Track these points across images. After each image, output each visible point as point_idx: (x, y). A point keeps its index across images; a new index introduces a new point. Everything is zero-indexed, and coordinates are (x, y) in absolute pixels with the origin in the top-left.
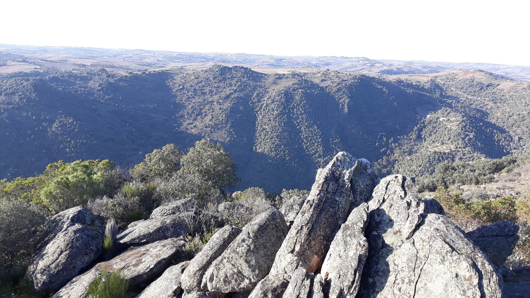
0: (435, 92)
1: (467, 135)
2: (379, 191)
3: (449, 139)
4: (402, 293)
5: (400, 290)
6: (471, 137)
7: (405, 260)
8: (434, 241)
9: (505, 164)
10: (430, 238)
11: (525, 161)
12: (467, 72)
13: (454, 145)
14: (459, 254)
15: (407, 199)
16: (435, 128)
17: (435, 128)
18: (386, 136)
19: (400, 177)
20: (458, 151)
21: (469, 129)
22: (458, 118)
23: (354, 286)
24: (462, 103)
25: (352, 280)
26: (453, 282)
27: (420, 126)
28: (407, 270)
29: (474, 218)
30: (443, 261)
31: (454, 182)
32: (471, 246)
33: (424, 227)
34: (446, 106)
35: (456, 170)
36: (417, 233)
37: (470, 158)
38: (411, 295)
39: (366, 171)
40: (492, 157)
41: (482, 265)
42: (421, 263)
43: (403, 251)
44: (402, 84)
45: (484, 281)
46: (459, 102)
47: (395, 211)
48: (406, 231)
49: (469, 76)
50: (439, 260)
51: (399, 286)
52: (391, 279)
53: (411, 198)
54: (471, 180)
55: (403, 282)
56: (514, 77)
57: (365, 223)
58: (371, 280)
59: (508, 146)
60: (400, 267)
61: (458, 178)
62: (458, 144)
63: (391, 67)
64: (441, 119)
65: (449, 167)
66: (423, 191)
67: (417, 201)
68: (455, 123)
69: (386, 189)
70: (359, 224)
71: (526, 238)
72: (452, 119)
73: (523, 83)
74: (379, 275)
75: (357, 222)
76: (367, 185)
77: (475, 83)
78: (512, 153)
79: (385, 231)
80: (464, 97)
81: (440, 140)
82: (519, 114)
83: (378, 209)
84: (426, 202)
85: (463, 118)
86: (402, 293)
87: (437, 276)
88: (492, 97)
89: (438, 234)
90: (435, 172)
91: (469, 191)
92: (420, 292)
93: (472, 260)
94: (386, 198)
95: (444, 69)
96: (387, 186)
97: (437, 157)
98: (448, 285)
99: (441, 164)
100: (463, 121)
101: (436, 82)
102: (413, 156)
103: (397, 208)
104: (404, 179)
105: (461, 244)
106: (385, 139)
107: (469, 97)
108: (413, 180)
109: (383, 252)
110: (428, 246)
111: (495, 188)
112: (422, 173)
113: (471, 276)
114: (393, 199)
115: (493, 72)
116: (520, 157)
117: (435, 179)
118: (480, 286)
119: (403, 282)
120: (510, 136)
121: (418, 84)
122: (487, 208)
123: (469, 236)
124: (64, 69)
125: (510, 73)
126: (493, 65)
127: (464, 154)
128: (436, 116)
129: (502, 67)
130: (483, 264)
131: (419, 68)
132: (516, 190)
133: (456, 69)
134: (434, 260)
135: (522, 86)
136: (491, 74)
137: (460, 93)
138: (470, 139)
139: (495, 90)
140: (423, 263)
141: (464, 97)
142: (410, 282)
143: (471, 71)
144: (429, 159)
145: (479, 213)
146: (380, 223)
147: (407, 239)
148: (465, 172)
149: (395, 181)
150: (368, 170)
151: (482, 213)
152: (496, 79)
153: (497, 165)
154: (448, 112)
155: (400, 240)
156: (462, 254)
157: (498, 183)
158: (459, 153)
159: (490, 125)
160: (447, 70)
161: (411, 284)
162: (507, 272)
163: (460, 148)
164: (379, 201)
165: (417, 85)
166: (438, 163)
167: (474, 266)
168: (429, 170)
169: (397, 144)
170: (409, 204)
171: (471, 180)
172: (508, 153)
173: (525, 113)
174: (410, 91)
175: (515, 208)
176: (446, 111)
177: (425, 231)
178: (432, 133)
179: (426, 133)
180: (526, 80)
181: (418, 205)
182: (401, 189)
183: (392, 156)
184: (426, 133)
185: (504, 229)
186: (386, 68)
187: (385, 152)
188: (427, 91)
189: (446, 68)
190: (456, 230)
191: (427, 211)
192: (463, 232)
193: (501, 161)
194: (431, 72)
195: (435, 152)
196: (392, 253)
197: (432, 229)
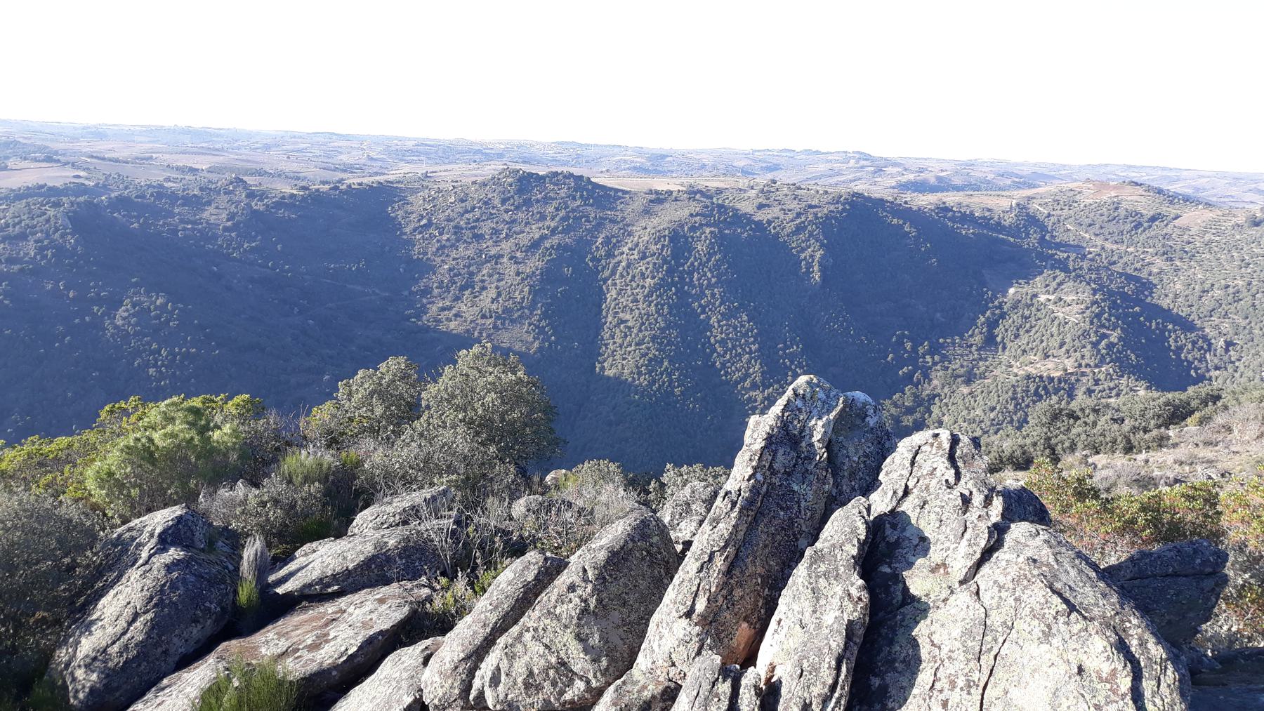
0: (1028, 235)
2: (894, 470)
3: (1062, 345)
6: (1114, 339)
7: (956, 632)
8: (1026, 588)
9: (1194, 404)
11: (1242, 399)
12: (1102, 185)
13: (1072, 360)
14: (1085, 618)
15: (963, 487)
16: (1027, 318)
17: (1027, 318)
18: (910, 339)
19: (945, 435)
20: (1083, 374)
21: (1109, 320)
23: (836, 695)
24: (1092, 260)
25: (830, 681)
26: (1072, 686)
27: (993, 314)
28: (961, 658)
29: (1121, 532)
30: (1047, 635)
31: (1073, 448)
32: (1115, 599)
33: (1001, 556)
34: (1053, 268)
35: (1077, 418)
36: (985, 569)
37: (1111, 389)
39: (863, 420)
41: (1141, 645)
42: (995, 640)
43: (953, 611)
44: (950, 214)
47: (933, 516)
49: (1106, 197)
50: (1037, 633)
51: (942, 697)
52: (924, 678)
54: (1114, 442)
55: (953, 685)
56: (1214, 199)
57: (862, 545)
58: (876, 682)
59: (1200, 361)
60: (945, 650)
61: (1083, 437)
62: (1083, 357)
64: (1042, 298)
66: (1000, 469)
67: (986, 492)
68: (1076, 308)
69: (913, 463)
70: (847, 547)
71: (1245, 581)
72: (1069, 298)
73: (1234, 211)
74: (895, 670)
76: (866, 456)
77: (1122, 212)
78: (1210, 379)
79: (910, 565)
81: (1041, 348)
82: (1227, 287)
83: (893, 511)
84: (1007, 495)
85: (1094, 295)
87: (1035, 671)
88: (1163, 246)
89: (1036, 572)
91: (1109, 468)
93: (1117, 634)
94: (911, 485)
95: (1047, 178)
96: (914, 458)
97: (1032, 388)
99: (1042, 406)
100: (1094, 303)
102: (977, 386)
103: (937, 510)
104: (955, 441)
105: (1090, 594)
106: (908, 346)
107: (1108, 246)
108: (976, 442)
109: (904, 615)
110: (1011, 601)
112: (997, 426)
114: (927, 488)
116: (1230, 387)
117: (1028, 441)
119: (953, 685)
120: (1205, 338)
121: (987, 214)
122: (1152, 509)
123: (1108, 575)
126: (1164, 169)
127: (1097, 382)
128: (1030, 290)
129: (1186, 173)
130: (1143, 644)
131: (990, 177)
132: (1220, 466)
133: (1076, 181)
134: (1026, 635)
136: (1160, 191)
137: (1087, 236)
138: (1110, 346)
139: (1168, 230)
140: (1001, 640)
141: (1096, 246)
142: (969, 685)
144: (1015, 393)
145: (1133, 521)
146: (897, 544)
147: (962, 583)
149: (932, 445)
150: (868, 419)
151: (1141, 521)
152: (1171, 202)
153: (1176, 408)
154: (1058, 280)
155: (944, 585)
156: (1092, 619)
157: (1177, 450)
158: (1084, 379)
161: (972, 691)
162: (1200, 662)
163: (1087, 365)
164: (895, 493)
165: (984, 218)
166: (1034, 402)
167: (1122, 646)
168: (1015, 418)
169: (937, 358)
170: (966, 501)
171: (1114, 442)
172: (1201, 379)
173: (1240, 282)
174: (967, 231)
175: (1219, 508)
176: (1054, 278)
177: (1004, 563)
178: (1022, 332)
180: (1241, 205)
181: (988, 501)
182: (947, 464)
185: (1193, 559)
186: (911, 177)
187: (910, 376)
188: (1008, 230)
189: (1053, 177)
190: (1077, 562)
191: (1010, 515)
192: (1094, 567)
193: (1184, 396)
194: (1019, 186)
195: (1028, 377)
197: (1021, 559)
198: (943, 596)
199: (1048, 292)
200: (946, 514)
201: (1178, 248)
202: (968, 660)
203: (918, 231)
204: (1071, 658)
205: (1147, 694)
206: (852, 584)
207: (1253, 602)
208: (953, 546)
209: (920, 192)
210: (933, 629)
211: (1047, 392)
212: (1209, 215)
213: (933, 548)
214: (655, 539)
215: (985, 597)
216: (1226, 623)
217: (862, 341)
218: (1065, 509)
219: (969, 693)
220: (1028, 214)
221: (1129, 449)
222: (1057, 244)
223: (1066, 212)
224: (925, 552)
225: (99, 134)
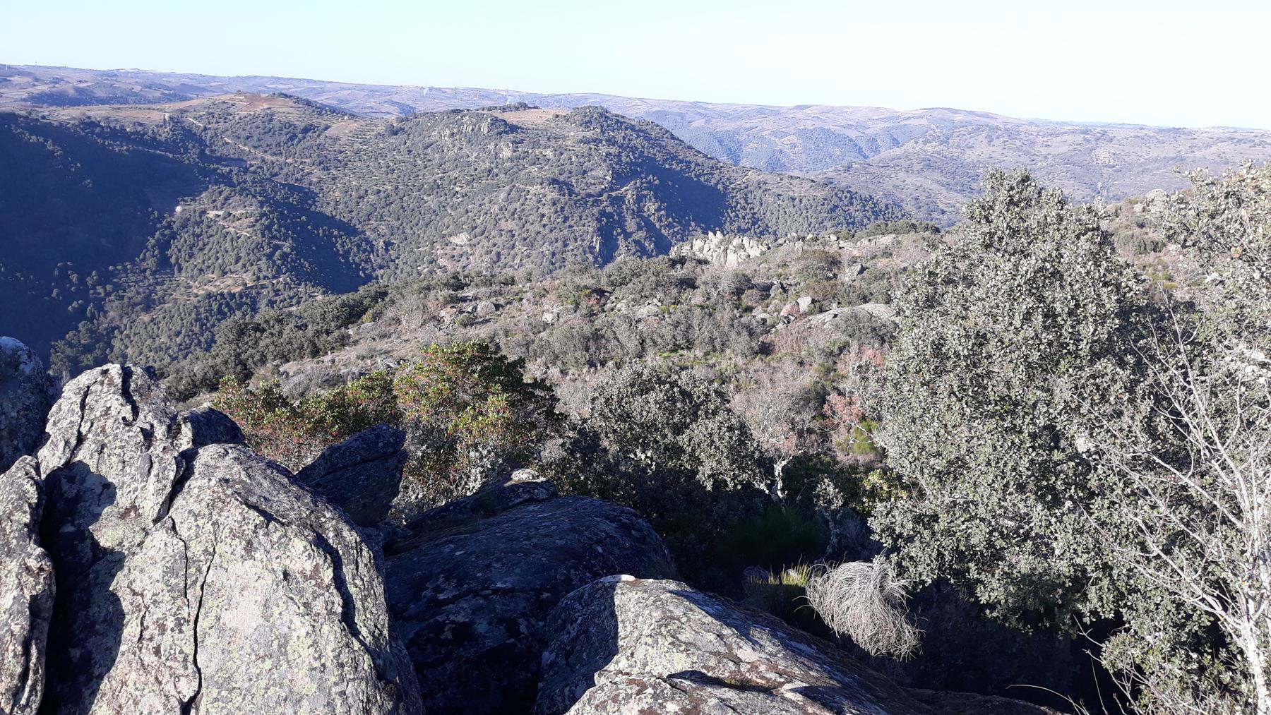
0: (186, 150)
1: (277, 247)
2: (63, 417)
4: (163, 658)
5: (157, 651)
6: (286, 249)
7: (157, 573)
8: (222, 510)
10: (211, 506)
11: (405, 292)
12: (254, 98)
14: (283, 524)
15: (142, 422)
16: (198, 236)
17: (198, 236)
18: (75, 270)
19: (114, 369)
21: (279, 231)
22: (250, 210)
23: (29, 682)
24: (255, 172)
25: (19, 670)
26: (280, 593)
27: (163, 235)
28: (167, 598)
29: (312, 433)
31: (263, 360)
32: (308, 499)
33: (194, 483)
34: (217, 183)
35: (263, 330)
36: (179, 501)
37: (291, 298)
38: (187, 656)
39: (17, 368)
42: (199, 570)
43: (151, 553)
44: (98, 130)
46: (246, 170)
48: (150, 504)
49: (260, 108)
50: (240, 551)
51: (152, 645)
52: (131, 630)
53: (150, 418)
54: (301, 348)
55: (162, 629)
56: (357, 110)
57: (34, 509)
58: (76, 653)
59: (366, 262)
60: (148, 595)
61: (272, 348)
62: (260, 270)
64: (211, 214)
65: (246, 325)
66: (194, 394)
67: (168, 422)
68: (246, 222)
70: (17, 516)
71: (423, 452)
72: (238, 212)
73: (375, 121)
74: (96, 633)
75: (11, 514)
76: (28, 408)
78: (377, 278)
79: (96, 517)
82: (379, 192)
83: (68, 464)
84: (194, 420)
85: (262, 207)
86: (163, 658)
87: (243, 589)
88: (319, 156)
89: (229, 492)
91: (298, 374)
92: (209, 641)
93: (314, 531)
94: (84, 430)
95: (199, 91)
96: (84, 400)
97: (215, 307)
98: (271, 604)
100: (263, 215)
101: (186, 125)
102: (158, 313)
103: (118, 451)
104: (127, 374)
105: (285, 501)
106: (74, 277)
107: (268, 158)
108: (151, 372)
109: (97, 572)
110: (209, 527)
111: (353, 358)
112: (185, 350)
114: (103, 430)
115: (312, 99)
116: (393, 282)
117: (218, 361)
118: (339, 582)
119: (162, 629)
120: (367, 241)
121: (139, 129)
123: (305, 479)
125: (348, 101)
126: (309, 81)
127: (277, 293)
128: (197, 207)
129: (329, 86)
130: (338, 534)
131: (137, 88)
132: (395, 354)
133: (227, 93)
135: (376, 130)
136: (308, 103)
137: (246, 148)
138: (284, 256)
139: (321, 140)
140: (204, 569)
141: (256, 159)
142: (179, 625)
143: (263, 95)
144: (198, 314)
145: (322, 420)
146: (78, 498)
147: (155, 521)
149: (102, 383)
150: (22, 366)
151: (329, 419)
152: (320, 114)
154: (224, 195)
155: (137, 529)
156: (289, 524)
157: (358, 347)
158: (265, 292)
160: (206, 94)
161: (184, 628)
162: (395, 533)
163: (265, 277)
164: (67, 443)
165: (137, 133)
166: (219, 321)
167: (320, 542)
169: (109, 287)
170: (148, 435)
171: (301, 348)
172: (369, 278)
173: (389, 188)
174: (121, 148)
175: (394, 393)
176: (220, 193)
177: (196, 491)
178: (195, 250)
179: (179, 251)
180: (379, 116)
181: (173, 432)
182: (121, 400)
183: (102, 318)
185: (377, 443)
186: (45, 88)
187: (82, 310)
188: (165, 145)
189: (204, 89)
190: (268, 472)
192: (286, 472)
193: (356, 296)
194: (169, 99)
195: (209, 296)
196: (122, 567)
197: (213, 482)
198: (138, 539)
199: (216, 208)
200: (128, 455)
201: (332, 157)
202: (175, 599)
203: (63, 149)
204: (275, 566)
205: (348, 578)
206: (29, 556)
207: (431, 468)
208: (140, 486)
210: (132, 577)
211: (230, 309)
212: (354, 125)
213: (119, 493)
214: (623, 482)
215: (183, 530)
216: (413, 493)
218: (257, 421)
219: (181, 631)
221: (316, 353)
222: (217, 158)
223: (222, 125)
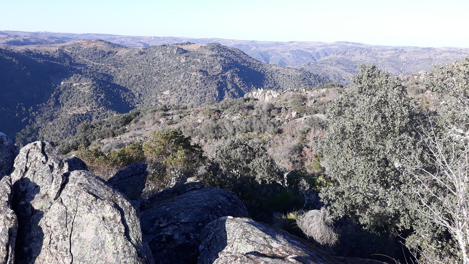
0: (65, 61)
2: (20, 161)
3: (84, 101)
4: (59, 250)
5: (56, 248)
6: (102, 97)
7: (56, 219)
8: (79, 195)
9: (132, 116)
10: (75, 193)
11: (147, 112)
12: (89, 42)
13: (89, 106)
14: (102, 200)
15: (49, 163)
16: (70, 93)
17: (70, 93)
19: (39, 143)
20: (94, 111)
22: (89, 83)
23: (9, 260)
24: (90, 69)
25: (5, 256)
26: (102, 225)
27: (57, 93)
28: (59, 228)
29: (113, 165)
30: (90, 210)
31: (94, 139)
32: (111, 190)
33: (69, 185)
34: (76, 73)
35: (94, 127)
36: (63, 192)
37: (104, 115)
39: (2, 143)
40: (122, 112)
41: (122, 204)
42: (71, 217)
43: (53, 211)
44: (32, 54)
45: (125, 216)
46: (87, 68)
47: (39, 176)
48: (53, 193)
49: (92, 45)
50: (86, 210)
51: (54, 245)
52: (46, 240)
53: (52, 161)
54: (108, 134)
55: (58, 239)
56: (128, 46)
57: (10, 196)
58: (26, 249)
59: (132, 102)
60: (52, 227)
61: (97, 134)
62: (93, 105)
63: (17, 38)
64: (74, 85)
65: (88, 126)
66: (69, 151)
67: (59, 162)
68: (87, 87)
69: (27, 157)
70: (3, 198)
72: (84, 84)
74: (34, 241)
76: (6, 158)
77: (98, 51)
78: (136, 107)
79: (33, 198)
80: (91, 64)
81: (77, 103)
82: (136, 75)
83: (22, 179)
84: (69, 161)
85: (93, 82)
86: (59, 250)
87: (87, 224)
88: (114, 63)
89: (82, 188)
90: (77, 132)
91: (107, 144)
92: (75, 243)
93: (114, 202)
94: (28, 166)
95: (69, 39)
96: (27, 155)
97: (76, 119)
99: (81, 125)
100: (93, 85)
102: (55, 121)
103: (40, 173)
104: (43, 145)
105: (103, 191)
106: (24, 109)
107: (95, 64)
109: (34, 219)
110: (75, 201)
111: (128, 137)
112: (66, 135)
113: (115, 215)
114: (35, 166)
115: (111, 41)
116: (142, 109)
117: (78, 139)
118: (123, 221)
119: (58, 239)
121: (47, 53)
122: (122, 155)
124: (264, 45)
125: (124, 42)
126: (110, 35)
127: (99, 113)
129: (117, 37)
130: (123, 203)
131: (46, 39)
132: (143, 136)
133: (80, 40)
134: (82, 212)
136: (110, 43)
137: (87, 60)
138: (102, 100)
139: (114, 57)
140: (73, 217)
141: (91, 64)
142: (64, 238)
143: (93, 40)
144: (70, 122)
145: (116, 161)
146: (26, 191)
147: (55, 199)
148: (102, 128)
149: (34, 148)
150: (4, 143)
153: (127, 118)
154: (79, 78)
155: (48, 202)
156: (104, 199)
158: (95, 113)
159: (116, 86)
161: (66, 239)
162: (144, 202)
164: (21, 171)
165: (46, 55)
166: (78, 124)
167: (116, 206)
168: (72, 131)
169: (37, 112)
170: (52, 167)
171: (108, 134)
172: (133, 108)
173: (140, 74)
174: (40, 61)
175: (143, 150)
176: (78, 77)
177: (70, 188)
178: (69, 98)
179: (63, 98)
180: (136, 47)
183: (34, 124)
184: (63, 98)
186: (12, 39)
188: (57, 60)
189: (71, 39)
190: (96, 180)
191: (71, 169)
192: (103, 180)
194: (58, 42)
195: (74, 115)
197: (76, 184)
199: (76, 82)
203: (19, 61)
204: (99, 215)
205: (127, 219)
206: (8, 213)
208: (49, 186)
209: (17, 45)
210: (46, 220)
212: (127, 51)
213: (41, 189)
215: (65, 202)
216: (150, 187)
217: (3, 110)
218: (92, 161)
219: (65, 240)
220: (63, 53)
221: (114, 135)
223: (78, 52)
224: (38, 191)
225: (36, 39)
